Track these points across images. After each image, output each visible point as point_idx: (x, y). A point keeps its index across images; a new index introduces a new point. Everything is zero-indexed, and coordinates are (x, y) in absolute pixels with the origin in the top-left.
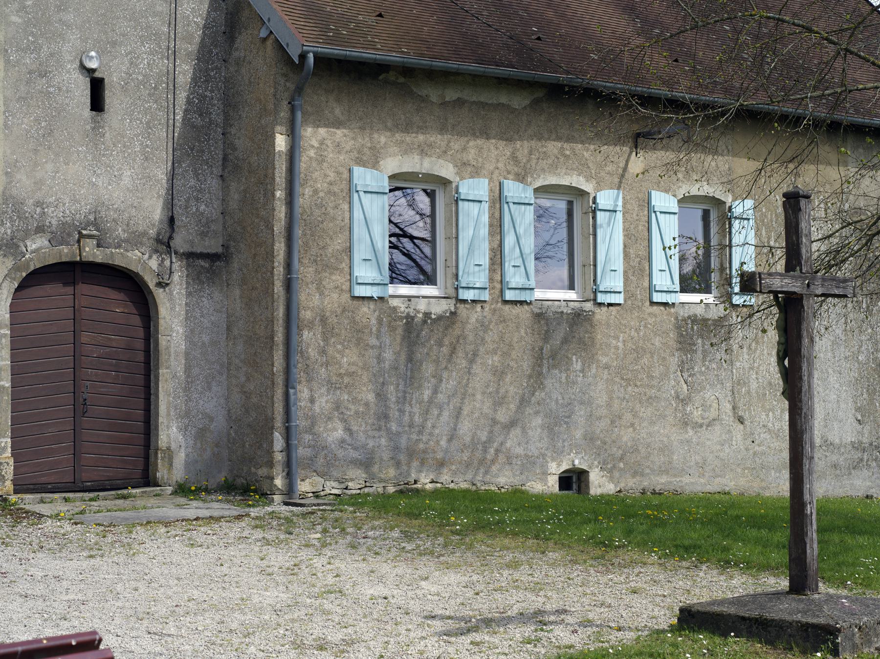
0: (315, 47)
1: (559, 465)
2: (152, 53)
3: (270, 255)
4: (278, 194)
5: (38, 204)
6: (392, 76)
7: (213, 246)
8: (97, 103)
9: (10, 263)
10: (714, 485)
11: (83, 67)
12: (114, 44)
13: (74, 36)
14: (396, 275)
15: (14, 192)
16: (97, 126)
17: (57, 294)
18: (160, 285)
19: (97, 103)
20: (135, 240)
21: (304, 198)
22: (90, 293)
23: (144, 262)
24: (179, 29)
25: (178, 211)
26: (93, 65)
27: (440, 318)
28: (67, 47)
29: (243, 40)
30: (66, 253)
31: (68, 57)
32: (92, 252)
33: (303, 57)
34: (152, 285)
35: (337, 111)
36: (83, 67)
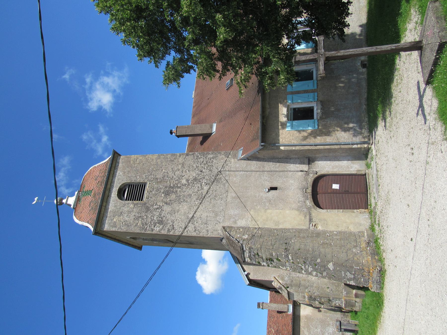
0: (259, 141)
1: (360, 69)
2: (263, 176)
3: (309, 150)
4: (294, 149)
5: (299, 202)
6: (264, 121)
7: (306, 161)
8: (275, 189)
9: (313, 209)
10: (395, 80)
11: (268, 192)
12: (262, 185)
13: (261, 194)
14: (312, 117)
15: (296, 208)
16: (281, 189)
17: (320, 198)
18: (316, 174)
19: (275, 189)
20: (306, 180)
21: (295, 142)
22: (319, 189)
23: (311, 178)
24: (258, 170)
25: (299, 170)
26: (267, 190)
27: (322, 105)
28: (264, 195)
29: (259, 156)
30: (310, 196)
31: (266, 195)
32: (310, 190)
33: (262, 146)
34: (316, 176)
35: (274, 135)
36: (268, 192)
